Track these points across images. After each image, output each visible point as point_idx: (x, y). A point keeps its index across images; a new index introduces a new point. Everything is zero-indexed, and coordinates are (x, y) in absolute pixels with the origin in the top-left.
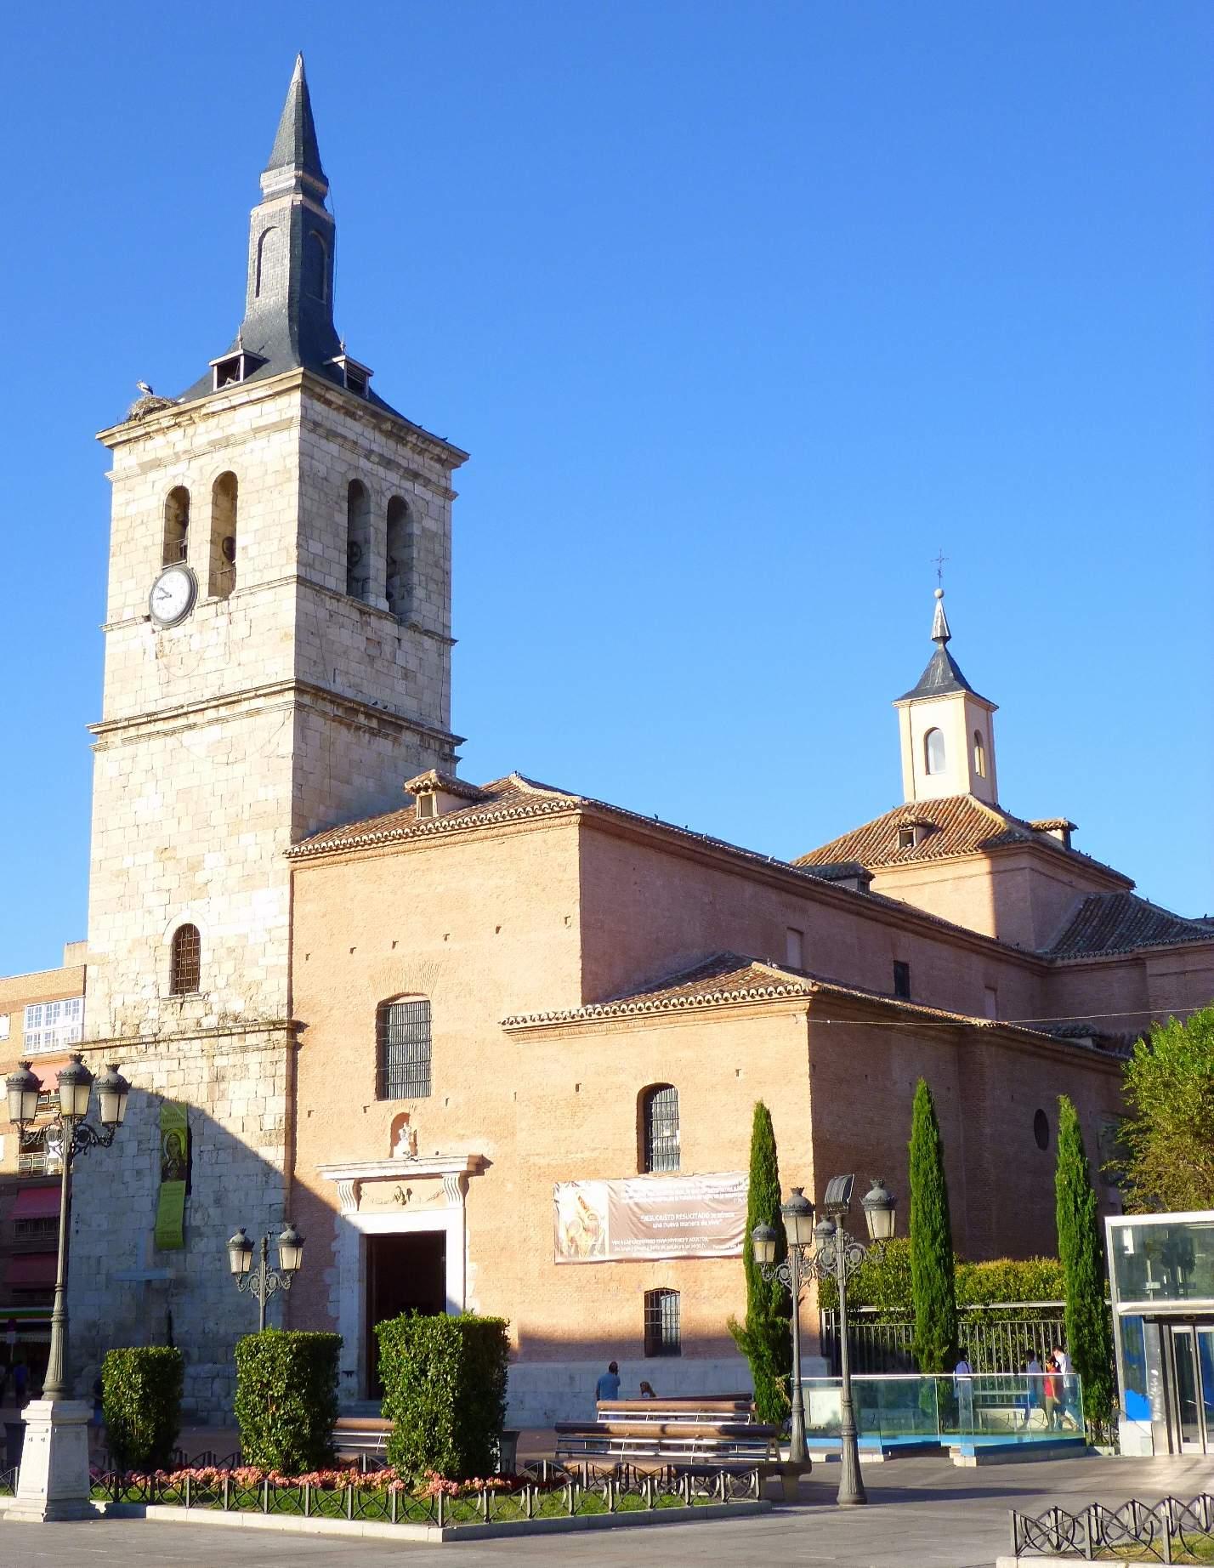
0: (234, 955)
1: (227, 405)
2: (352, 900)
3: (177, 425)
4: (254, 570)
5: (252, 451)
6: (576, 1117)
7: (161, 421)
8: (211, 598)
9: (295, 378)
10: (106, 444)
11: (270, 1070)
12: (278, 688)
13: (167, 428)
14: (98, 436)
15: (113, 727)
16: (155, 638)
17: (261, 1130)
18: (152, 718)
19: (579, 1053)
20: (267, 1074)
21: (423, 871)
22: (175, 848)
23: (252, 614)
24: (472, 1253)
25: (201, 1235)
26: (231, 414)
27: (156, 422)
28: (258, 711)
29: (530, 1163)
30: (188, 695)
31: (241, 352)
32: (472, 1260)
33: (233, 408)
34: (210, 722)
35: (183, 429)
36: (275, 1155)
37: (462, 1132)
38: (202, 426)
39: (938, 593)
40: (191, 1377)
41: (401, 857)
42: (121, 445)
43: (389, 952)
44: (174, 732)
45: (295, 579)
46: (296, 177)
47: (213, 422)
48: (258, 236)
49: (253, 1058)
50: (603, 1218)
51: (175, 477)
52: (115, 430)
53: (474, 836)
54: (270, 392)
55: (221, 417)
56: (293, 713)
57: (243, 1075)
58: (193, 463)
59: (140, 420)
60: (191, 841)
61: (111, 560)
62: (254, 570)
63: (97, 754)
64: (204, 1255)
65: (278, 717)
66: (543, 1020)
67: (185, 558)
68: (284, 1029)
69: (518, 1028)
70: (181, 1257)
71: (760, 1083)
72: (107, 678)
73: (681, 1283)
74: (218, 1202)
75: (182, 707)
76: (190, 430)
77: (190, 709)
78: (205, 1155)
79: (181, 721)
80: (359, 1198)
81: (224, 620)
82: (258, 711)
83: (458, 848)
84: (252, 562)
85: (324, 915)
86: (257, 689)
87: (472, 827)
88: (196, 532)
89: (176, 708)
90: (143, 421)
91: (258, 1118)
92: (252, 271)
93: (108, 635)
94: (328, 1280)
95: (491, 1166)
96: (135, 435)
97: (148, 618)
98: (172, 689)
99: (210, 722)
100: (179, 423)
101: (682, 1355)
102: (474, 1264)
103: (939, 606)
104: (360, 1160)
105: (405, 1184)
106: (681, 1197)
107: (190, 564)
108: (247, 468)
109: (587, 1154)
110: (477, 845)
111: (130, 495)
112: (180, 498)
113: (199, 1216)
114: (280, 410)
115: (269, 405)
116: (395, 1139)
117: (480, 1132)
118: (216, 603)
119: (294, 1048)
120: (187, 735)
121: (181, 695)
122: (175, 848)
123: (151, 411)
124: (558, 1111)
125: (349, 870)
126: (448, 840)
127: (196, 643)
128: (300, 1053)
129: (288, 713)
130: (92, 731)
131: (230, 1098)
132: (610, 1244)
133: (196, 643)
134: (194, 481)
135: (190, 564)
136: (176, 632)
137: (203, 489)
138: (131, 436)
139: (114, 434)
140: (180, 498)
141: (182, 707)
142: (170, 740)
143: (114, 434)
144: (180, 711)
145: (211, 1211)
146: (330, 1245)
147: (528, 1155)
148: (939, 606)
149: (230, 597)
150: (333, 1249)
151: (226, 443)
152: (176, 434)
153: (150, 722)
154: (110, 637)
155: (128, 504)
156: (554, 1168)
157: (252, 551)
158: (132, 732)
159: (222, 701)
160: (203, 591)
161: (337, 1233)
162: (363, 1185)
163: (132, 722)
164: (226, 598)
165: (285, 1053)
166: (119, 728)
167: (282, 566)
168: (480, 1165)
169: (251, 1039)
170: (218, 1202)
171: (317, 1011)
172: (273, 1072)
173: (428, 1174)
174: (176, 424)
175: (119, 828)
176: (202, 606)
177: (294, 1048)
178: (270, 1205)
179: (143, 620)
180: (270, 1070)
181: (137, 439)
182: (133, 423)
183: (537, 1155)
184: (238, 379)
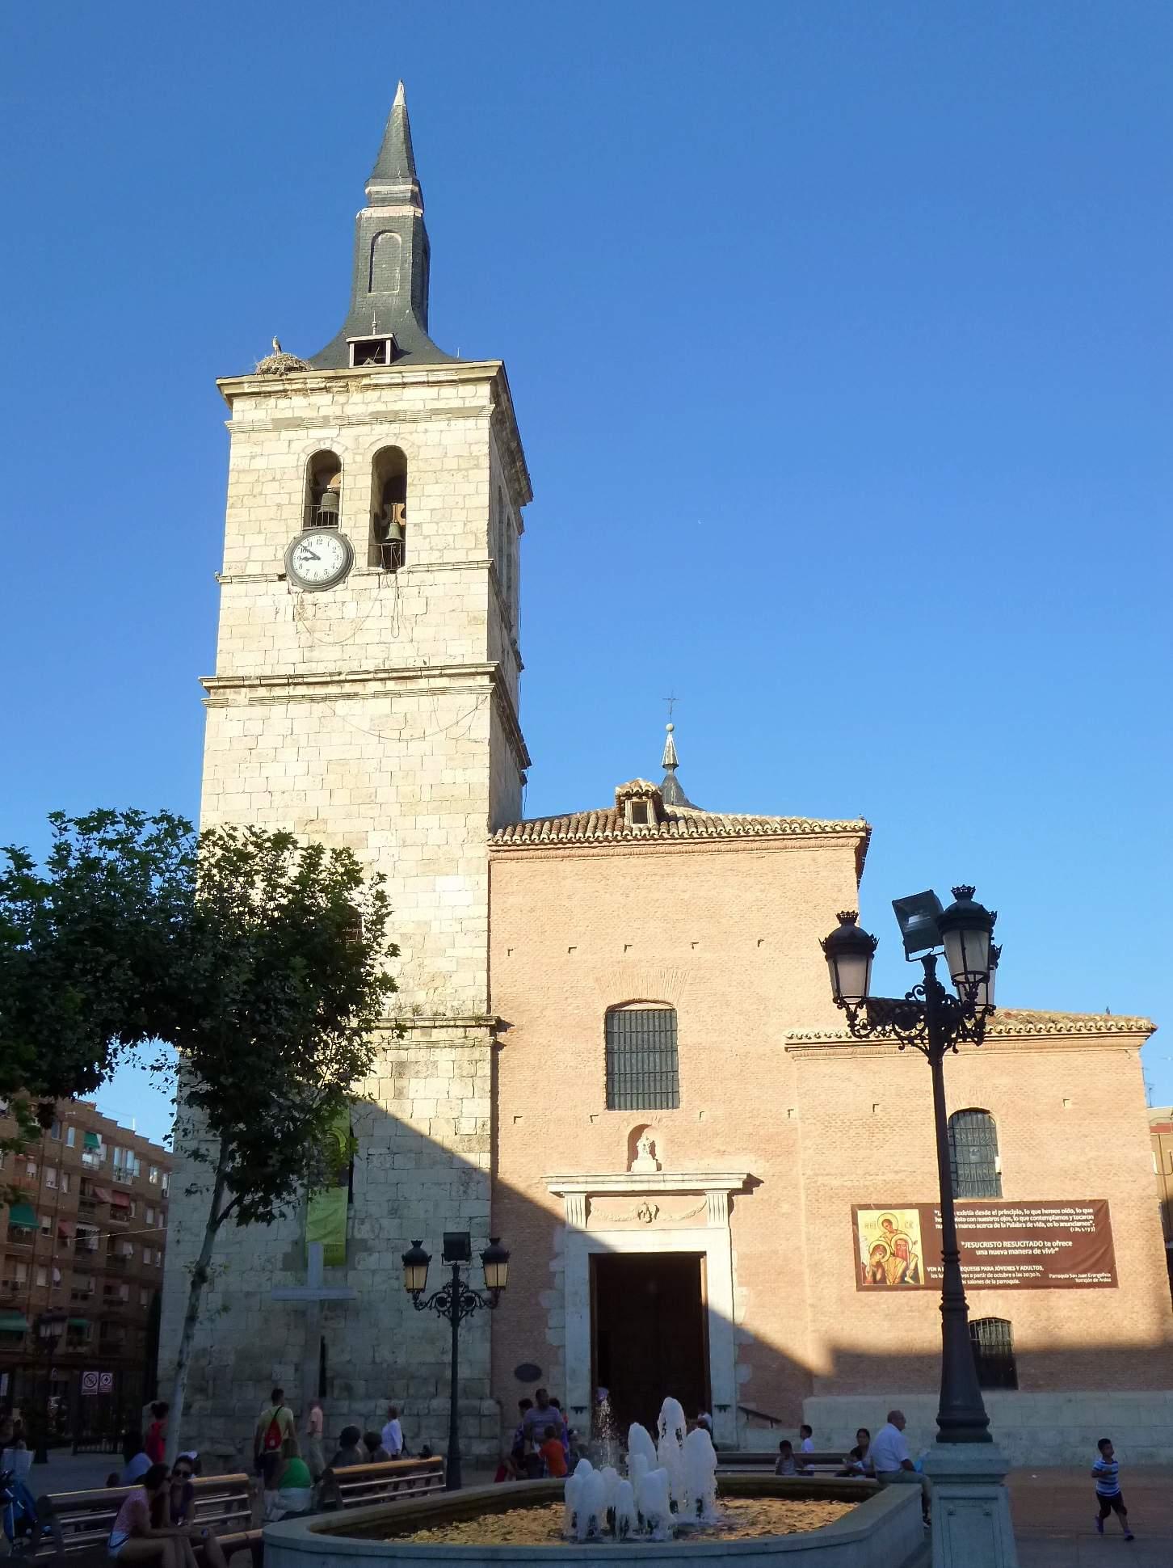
0: (411, 942)
1: (400, 381)
2: (569, 897)
3: (327, 389)
4: (431, 549)
5: (426, 431)
6: (874, 1139)
7: (308, 381)
8: (371, 568)
9: (490, 369)
10: (226, 392)
11: (468, 1069)
12: (473, 670)
13: (312, 390)
14: (219, 382)
15: (237, 683)
16: (292, 600)
17: (456, 1134)
18: (293, 680)
19: (874, 1073)
20: (465, 1074)
21: (663, 876)
22: (325, 821)
23: (427, 591)
24: (740, 1276)
25: (369, 1250)
26: (397, 391)
27: (301, 381)
28: (444, 691)
29: (819, 1184)
30: (339, 663)
31: (391, 336)
32: (741, 1284)
33: (404, 385)
34: (375, 695)
35: (331, 395)
36: (483, 1161)
37: (722, 1148)
38: (356, 397)
39: (669, 726)
40: (361, 1415)
41: (634, 860)
42: (245, 397)
43: (621, 955)
44: (325, 698)
45: (489, 565)
46: (412, 191)
47: (372, 395)
48: (370, 236)
49: (444, 1057)
50: (915, 1243)
51: (319, 440)
52: (244, 379)
53: (675, 848)
54: (456, 378)
55: (383, 392)
56: (489, 698)
57: (429, 1073)
58: (345, 431)
59: (280, 376)
60: (349, 816)
61: (228, 511)
62: (431, 549)
63: (210, 710)
64: (374, 1272)
65: (470, 700)
66: (810, 1038)
67: (337, 523)
68: (486, 1026)
69: (798, 1046)
70: (339, 1274)
71: (1091, 1114)
72: (223, 632)
73: (1013, 1312)
74: (394, 1212)
75: (340, 674)
76: (341, 398)
77: (350, 677)
78: (374, 1159)
79: (333, 690)
80: (588, 1212)
81: (389, 593)
82: (444, 691)
83: (707, 857)
84: (428, 540)
85: (532, 910)
86: (443, 668)
87: (734, 837)
88: (350, 500)
89: (331, 675)
90: (284, 377)
91: (453, 1121)
92: (363, 266)
93: (223, 587)
94: (545, 1303)
95: (761, 1185)
96: (268, 389)
97: (282, 577)
98: (316, 654)
99: (375, 695)
100: (330, 387)
101: (1020, 1388)
102: (744, 1290)
103: (670, 738)
104: (587, 1172)
105: (653, 1201)
106: (1008, 1224)
107: (342, 530)
108: (419, 447)
109: (890, 1177)
110: (729, 856)
111: (257, 450)
112: (324, 467)
113: (366, 1227)
114: (463, 398)
115: (448, 391)
116: (633, 1154)
117: (746, 1149)
118: (379, 574)
119: (496, 1047)
120: (341, 706)
121: (326, 661)
122: (325, 821)
123: (290, 369)
124: (851, 1131)
125: (566, 866)
126: (697, 847)
127: (350, 611)
128: (501, 1054)
129: (482, 697)
130: (205, 684)
131: (411, 1097)
132: (925, 1271)
133: (350, 611)
134: (347, 449)
135: (342, 530)
136: (322, 597)
137: (359, 458)
138: (264, 389)
139: (243, 383)
140: (324, 467)
141: (340, 674)
142: (319, 708)
143: (243, 383)
144: (336, 678)
145: (385, 1222)
146: (547, 1264)
147: (817, 1175)
148: (670, 738)
149: (399, 571)
150: (552, 1269)
151: (394, 418)
152: (325, 398)
153: (288, 684)
154: (225, 589)
155: (253, 457)
156: (849, 1189)
157: (427, 529)
158: (262, 692)
159: (395, 675)
160: (361, 560)
161: (429, 1255)
162: (593, 1201)
163: (263, 682)
164: (394, 572)
165: (489, 1052)
166: (244, 686)
167: (471, 549)
168: (751, 1184)
169: (437, 1035)
170: (394, 1212)
171: (524, 1011)
172: (473, 1071)
173: (686, 1195)
174: (325, 388)
175: (243, 792)
176: (360, 575)
177: (496, 1047)
178: (471, 1218)
179: (277, 578)
180: (468, 1069)
181: (269, 394)
182: (270, 377)
183: (827, 1175)
184: (383, 361)
